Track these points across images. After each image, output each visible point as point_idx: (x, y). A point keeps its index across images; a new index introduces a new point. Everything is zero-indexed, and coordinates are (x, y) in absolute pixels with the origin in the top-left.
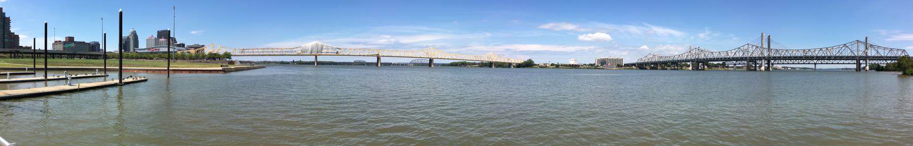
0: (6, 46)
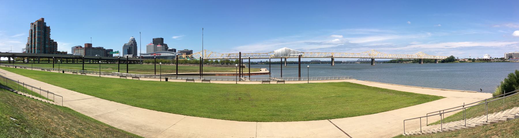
0: (47, 51)
